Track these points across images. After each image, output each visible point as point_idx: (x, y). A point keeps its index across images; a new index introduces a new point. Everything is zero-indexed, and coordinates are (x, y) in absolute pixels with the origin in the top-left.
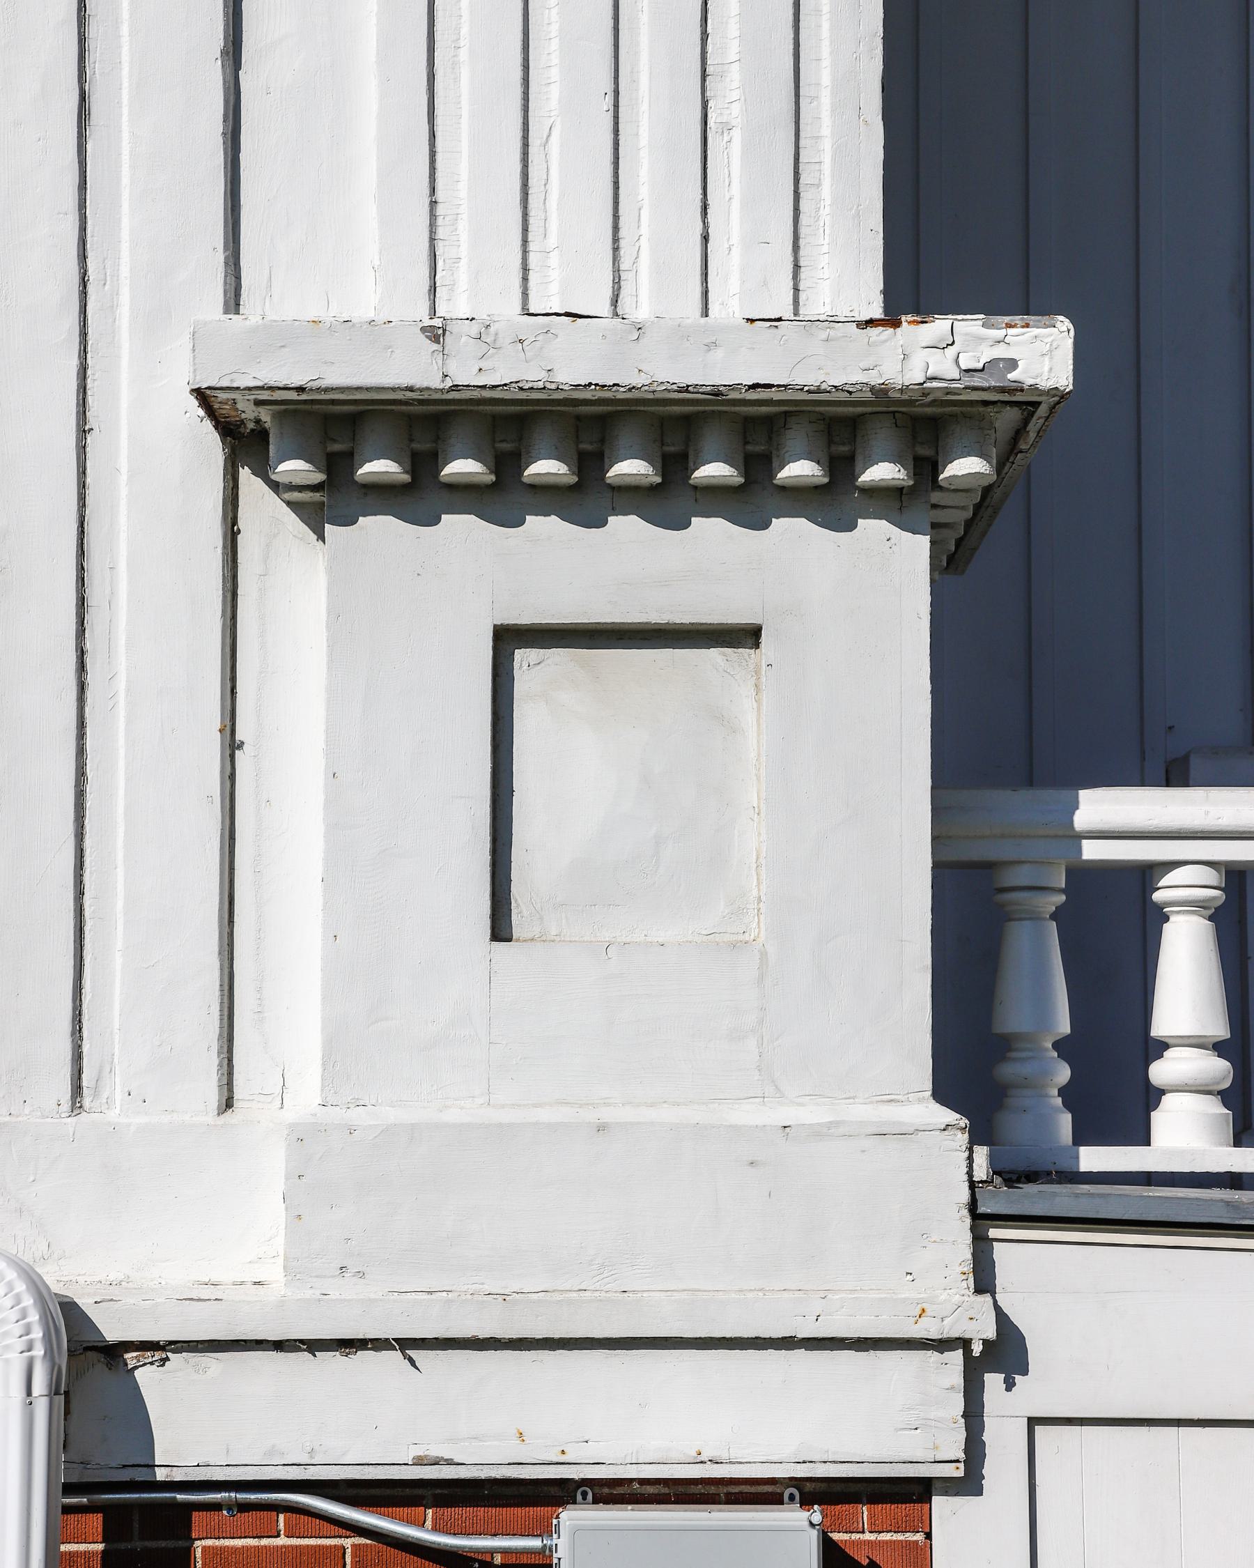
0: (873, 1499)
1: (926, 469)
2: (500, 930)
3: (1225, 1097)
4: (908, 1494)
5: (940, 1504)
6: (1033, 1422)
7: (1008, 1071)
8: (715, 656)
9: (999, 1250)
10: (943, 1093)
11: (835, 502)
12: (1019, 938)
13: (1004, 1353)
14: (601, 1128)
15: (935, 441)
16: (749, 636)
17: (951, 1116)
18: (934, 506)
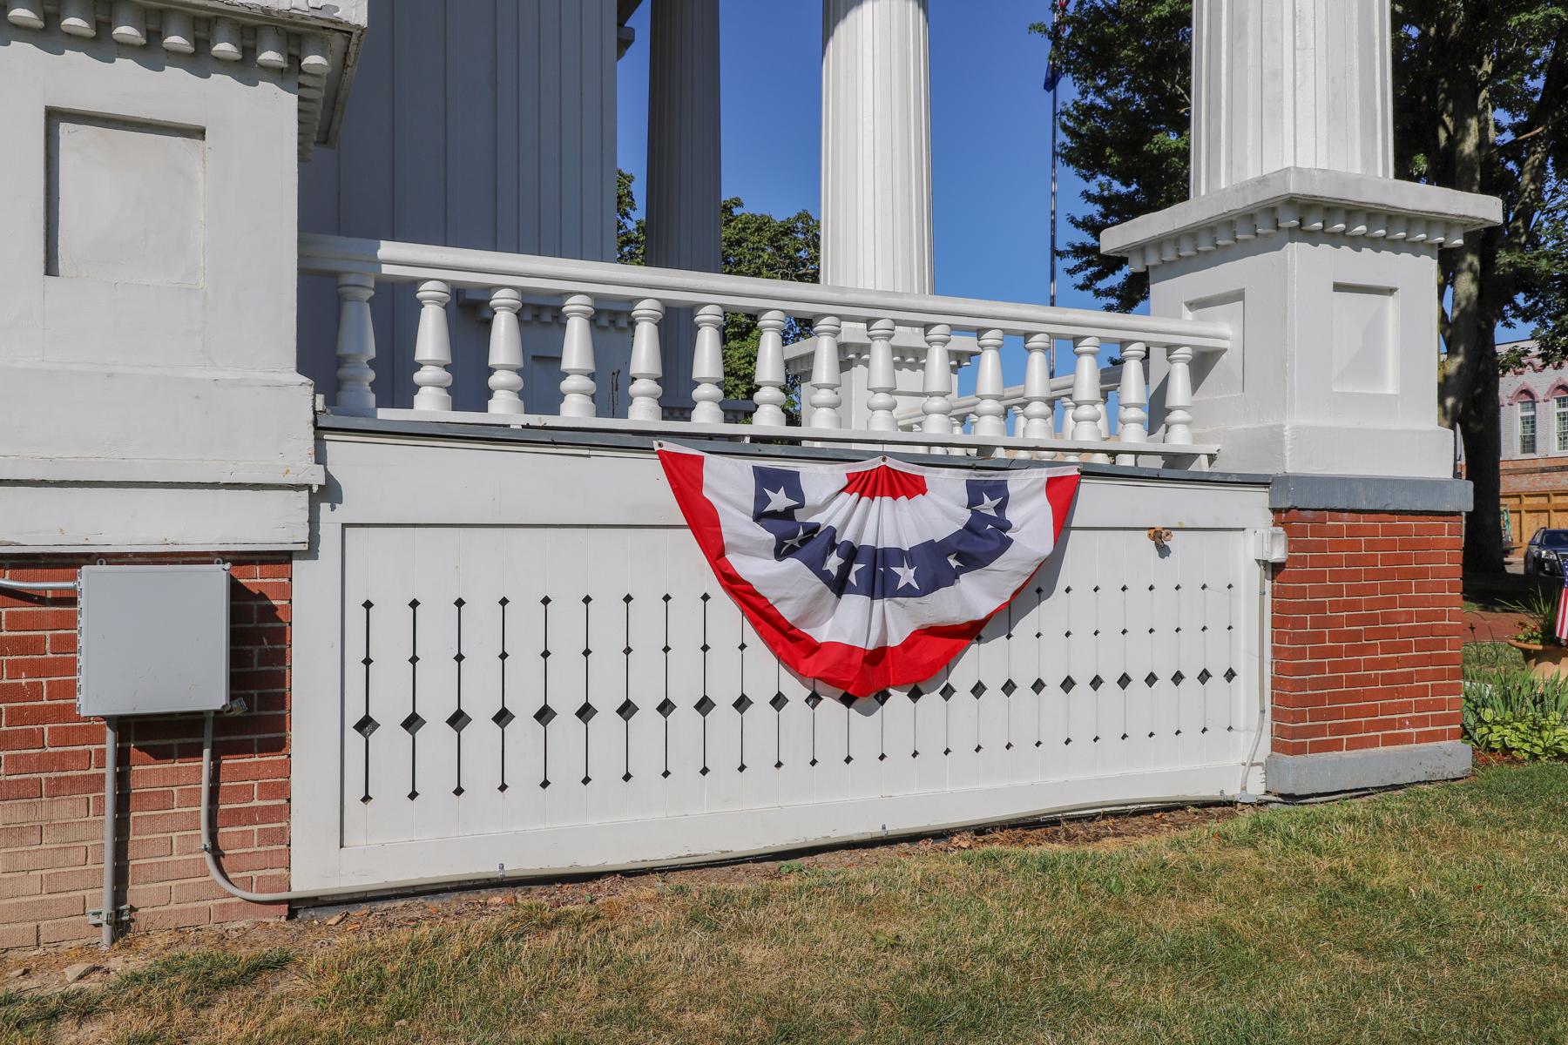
0: (262, 563)
1: (295, 60)
2: (51, 268)
3: (449, 390)
4: (281, 559)
5: (297, 564)
6: (344, 526)
7: (343, 372)
8: (180, 141)
9: (329, 445)
10: (301, 369)
11: (245, 68)
12: (350, 310)
13: (328, 492)
14: (110, 375)
15: (299, 46)
16: (199, 133)
17: (305, 379)
18: (300, 86)
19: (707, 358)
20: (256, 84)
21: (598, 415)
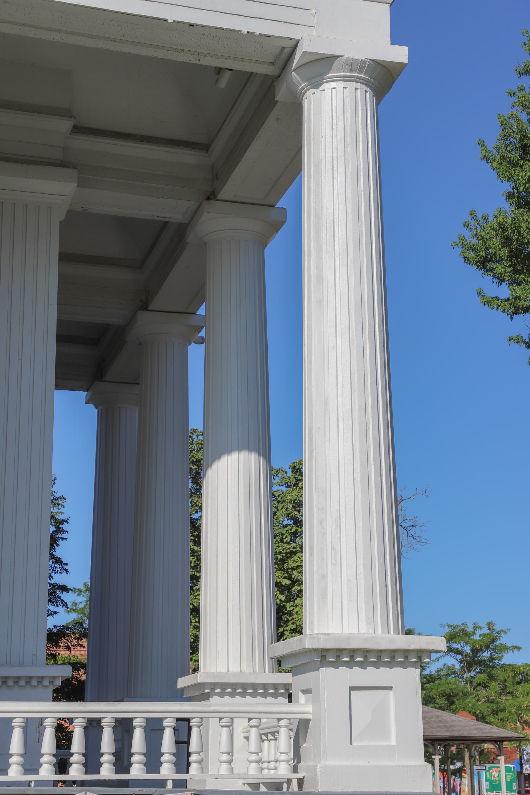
3: (145, 765)
19: (107, 743)
20: (406, 668)
21: (117, 773)
